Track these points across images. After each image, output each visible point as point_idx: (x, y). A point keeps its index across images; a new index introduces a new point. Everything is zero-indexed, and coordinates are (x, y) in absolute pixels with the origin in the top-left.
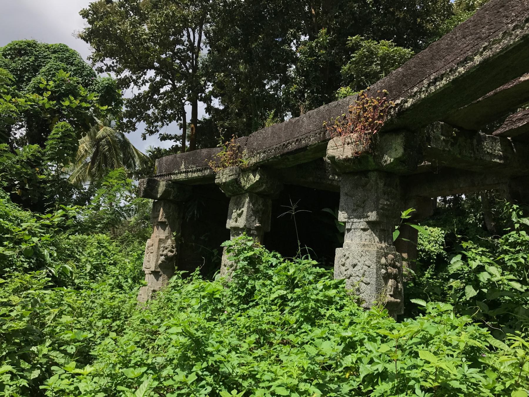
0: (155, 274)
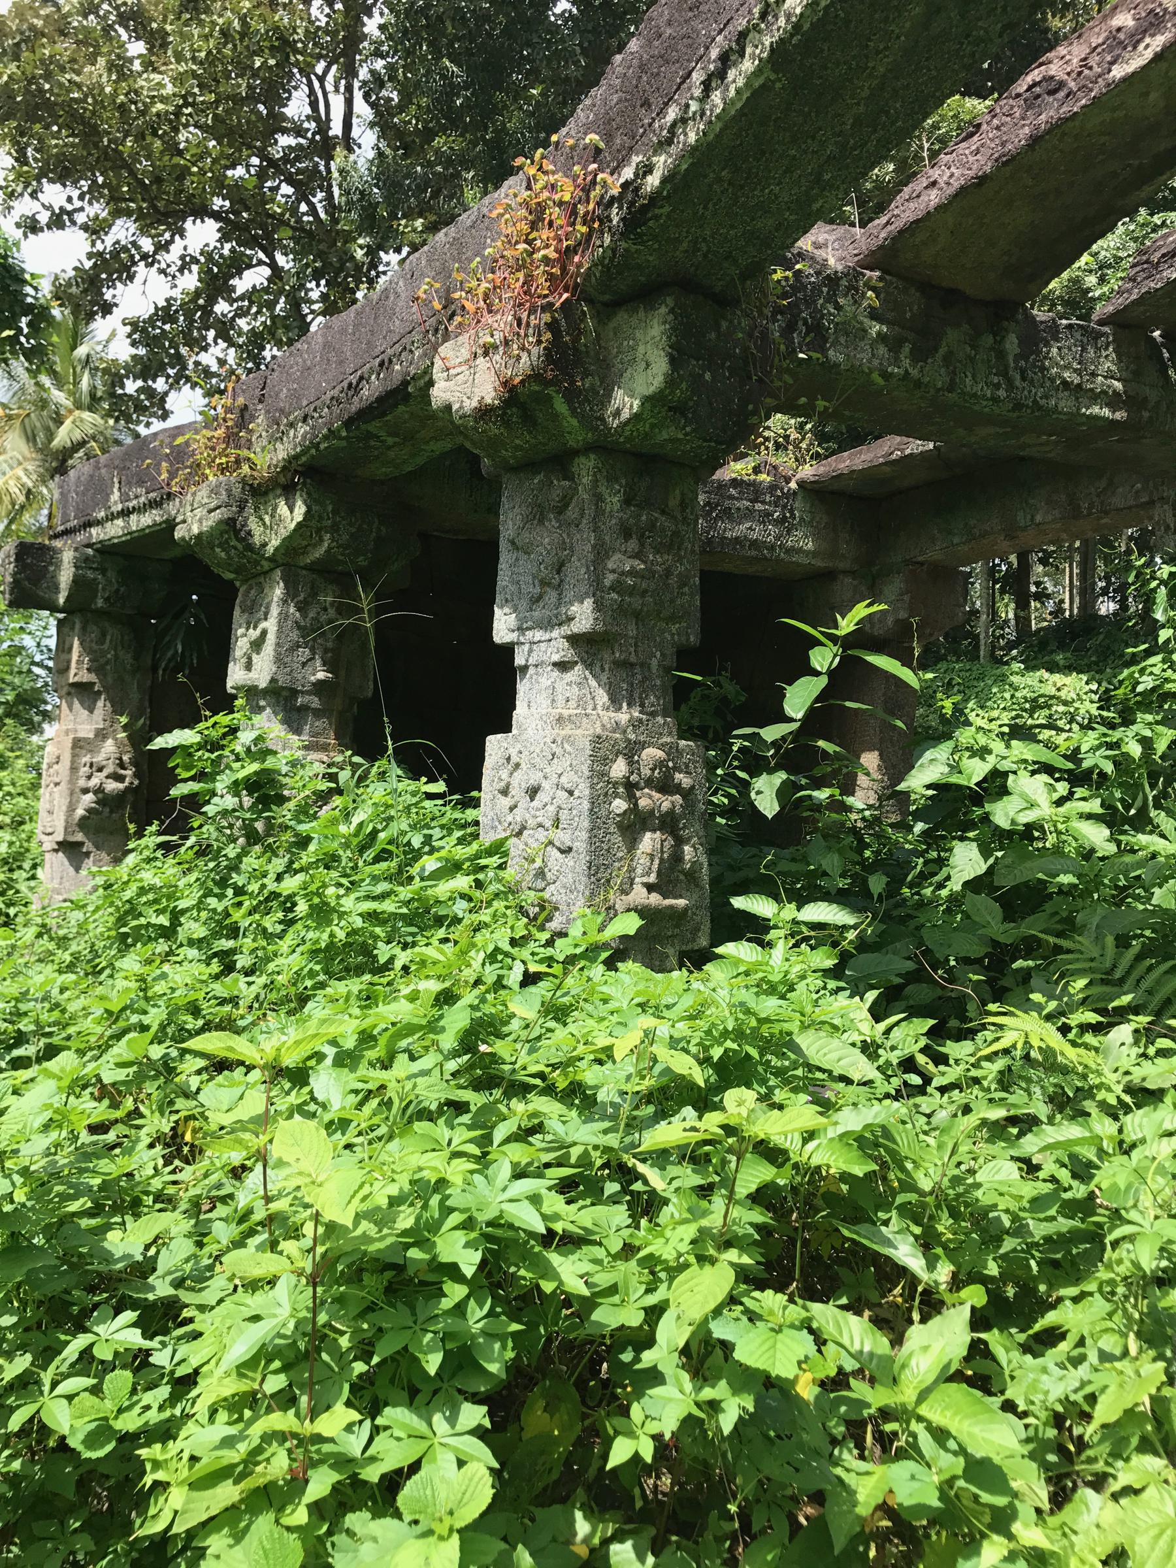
0: (68, 848)
